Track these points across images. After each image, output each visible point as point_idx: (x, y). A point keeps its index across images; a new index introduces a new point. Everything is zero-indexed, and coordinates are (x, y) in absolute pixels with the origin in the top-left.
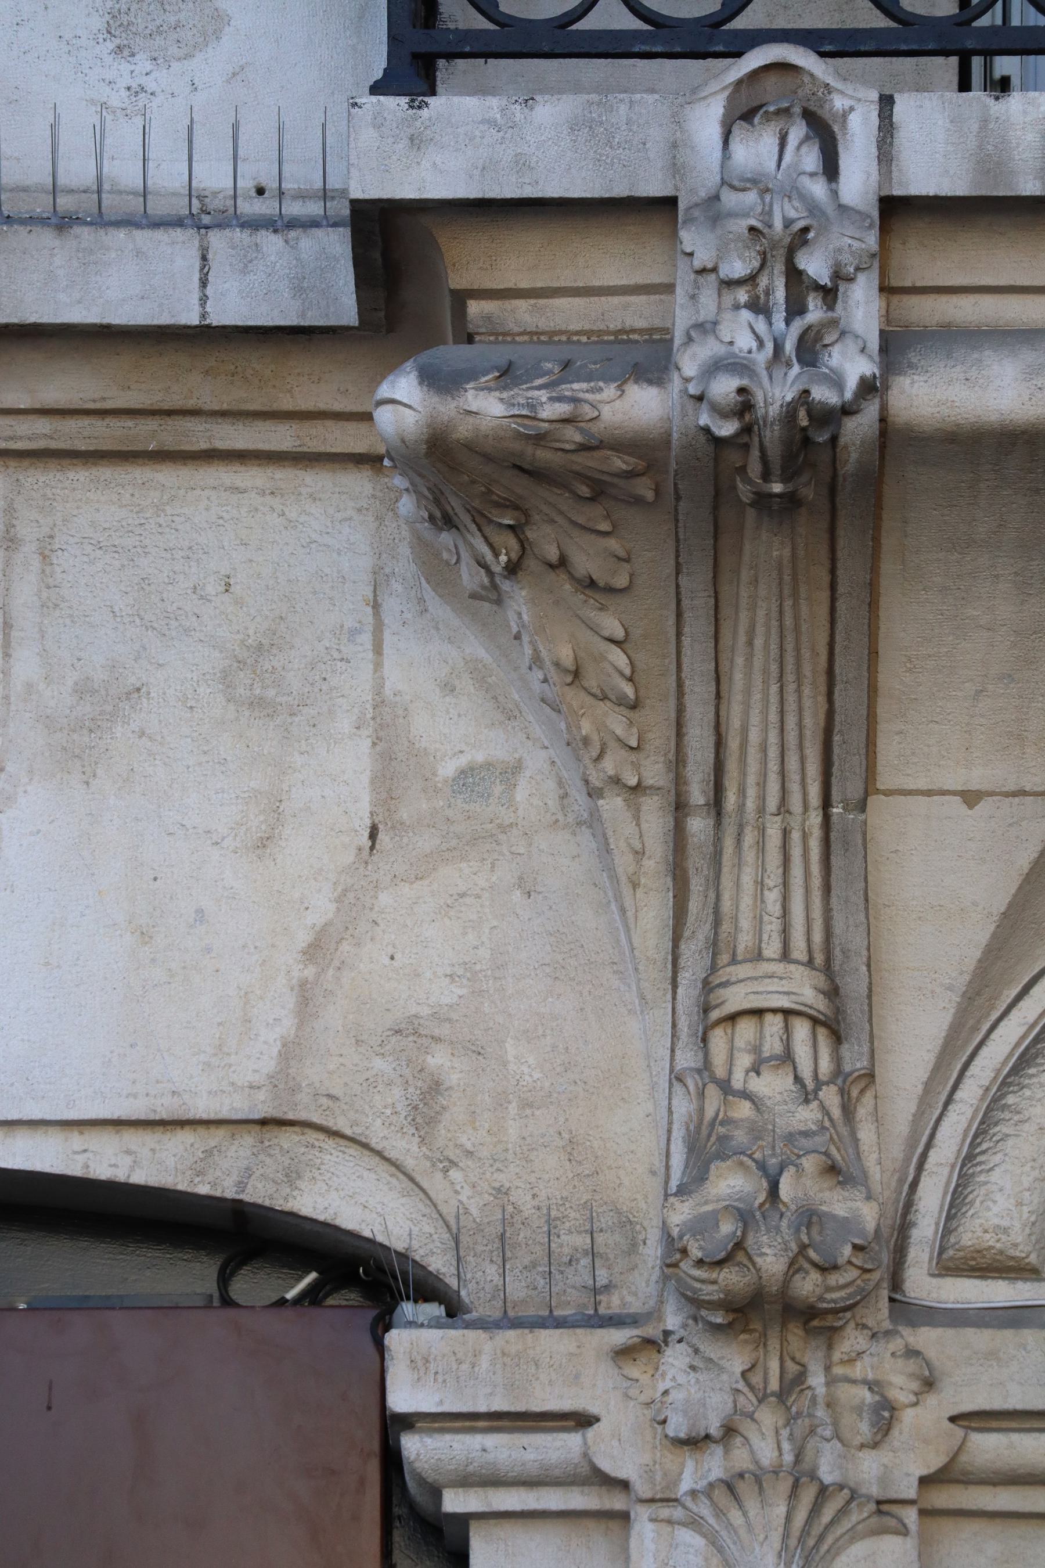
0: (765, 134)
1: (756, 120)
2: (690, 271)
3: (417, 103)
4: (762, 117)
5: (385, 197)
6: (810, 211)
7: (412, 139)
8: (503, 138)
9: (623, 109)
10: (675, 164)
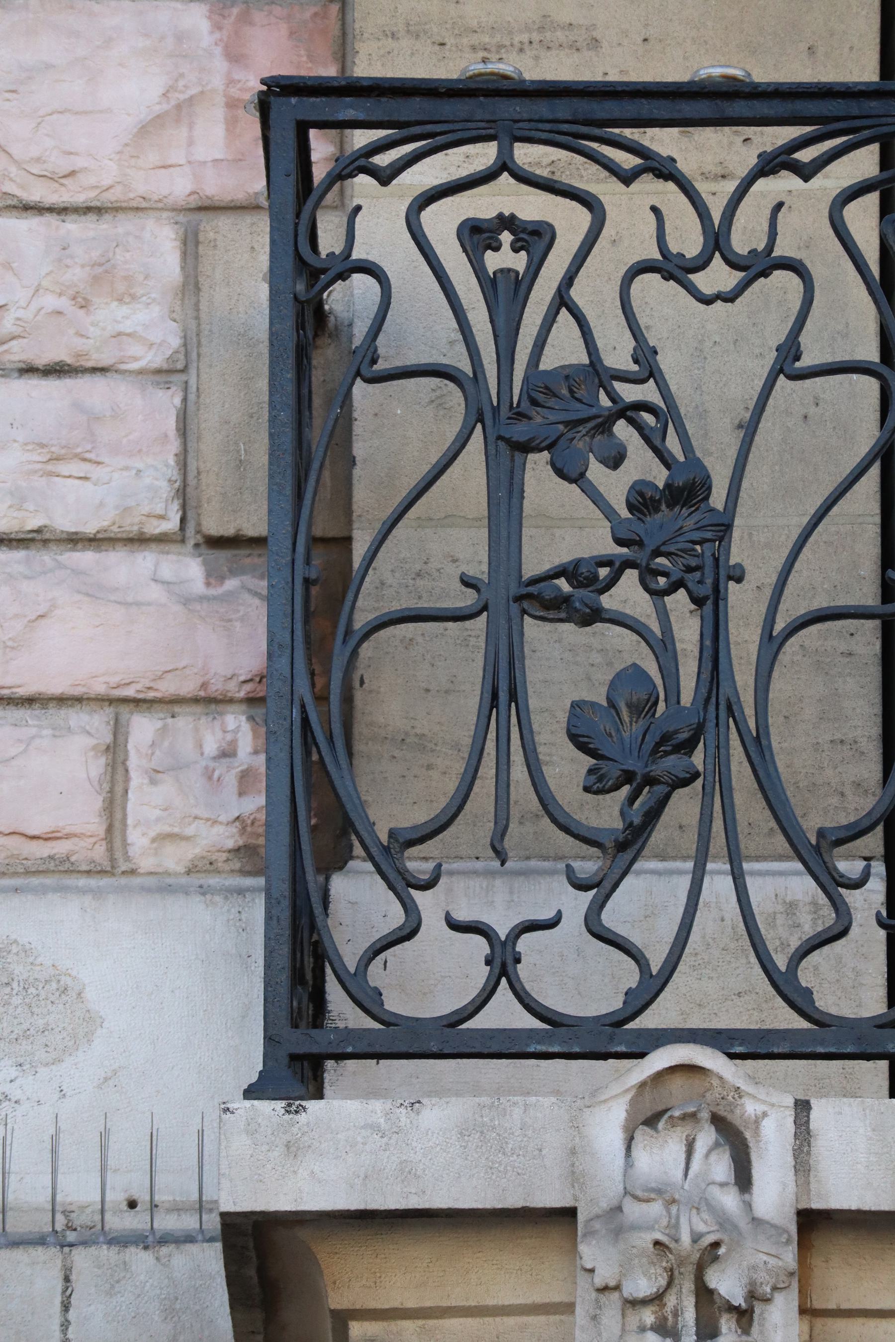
0: (670, 1141)
1: (661, 1125)
2: (592, 1289)
3: (294, 1108)
4: (666, 1122)
5: (258, 1209)
6: (721, 1224)
7: (288, 1146)
8: (387, 1144)
9: (517, 1112)
10: (573, 1173)
